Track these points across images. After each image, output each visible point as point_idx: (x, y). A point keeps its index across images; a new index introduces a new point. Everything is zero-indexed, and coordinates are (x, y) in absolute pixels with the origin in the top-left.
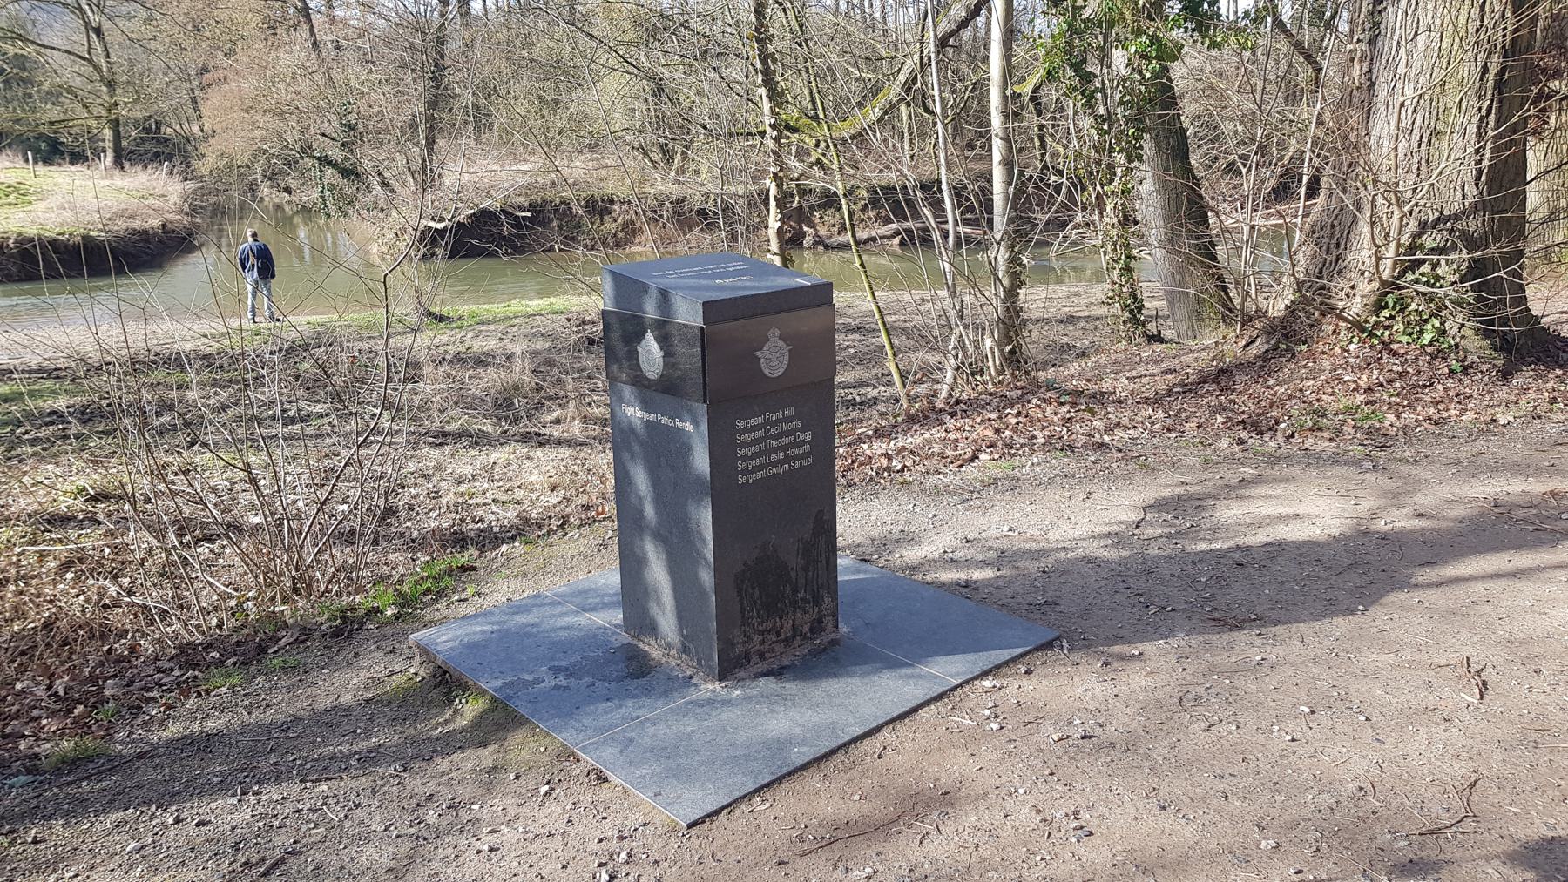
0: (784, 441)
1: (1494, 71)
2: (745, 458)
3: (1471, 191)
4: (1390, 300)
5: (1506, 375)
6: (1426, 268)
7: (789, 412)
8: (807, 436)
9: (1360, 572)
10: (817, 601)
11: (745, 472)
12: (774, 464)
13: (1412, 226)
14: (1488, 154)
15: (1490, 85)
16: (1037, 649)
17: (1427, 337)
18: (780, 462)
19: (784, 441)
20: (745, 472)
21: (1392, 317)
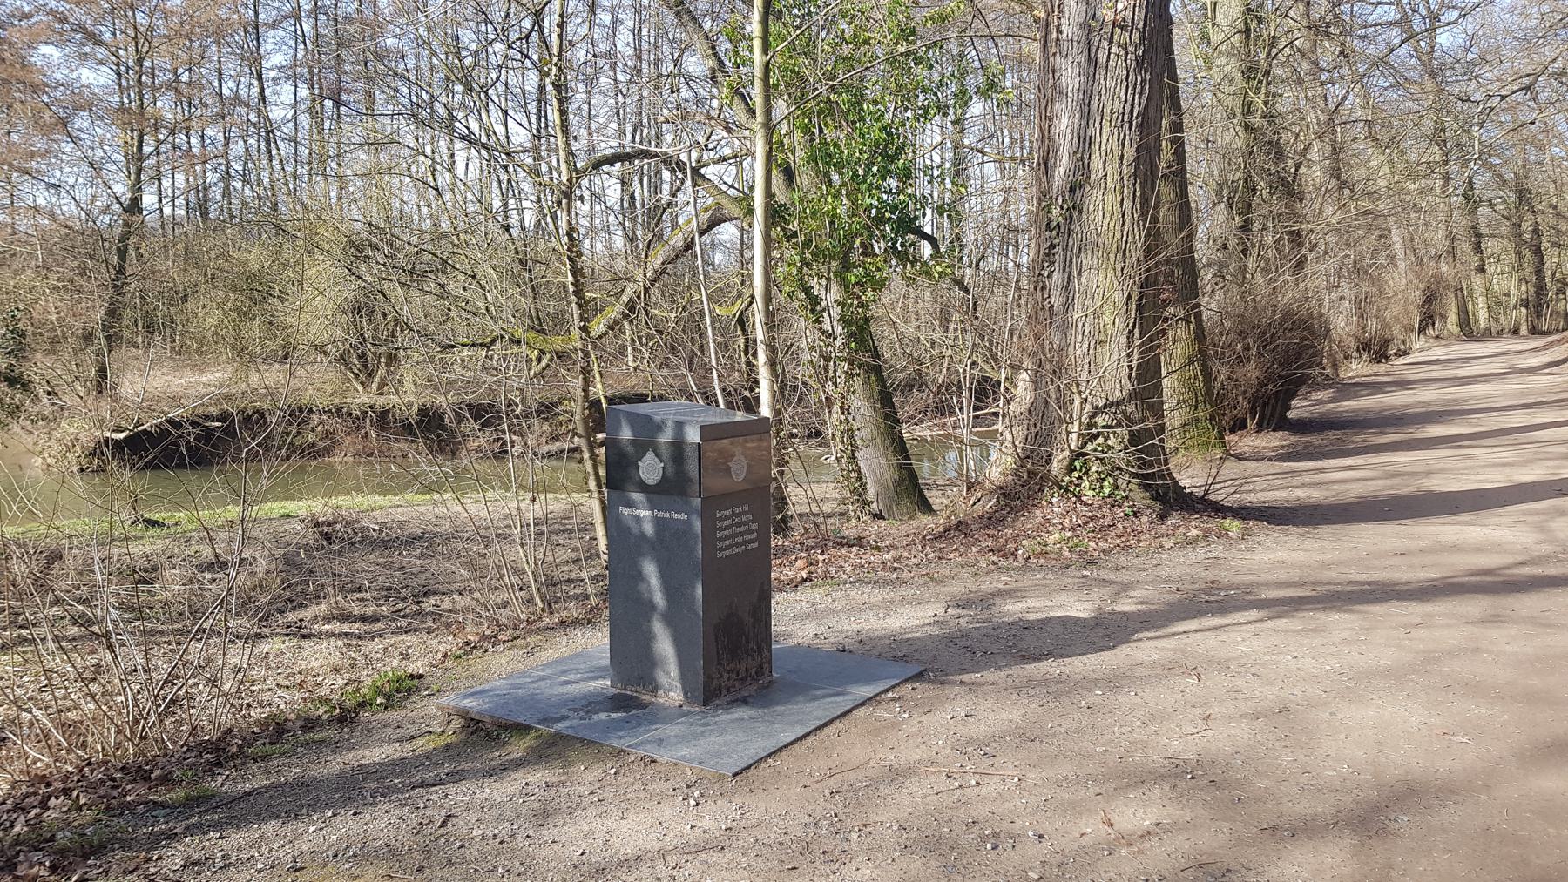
0: (742, 529)
1: (1135, 297)
2: (721, 539)
3: (1126, 383)
4: (1077, 464)
5: (1163, 517)
6: (1100, 440)
7: (746, 508)
8: (755, 526)
9: (1108, 631)
10: (760, 652)
11: (722, 549)
12: (737, 545)
13: (1088, 408)
14: (1136, 356)
15: (1134, 307)
16: (907, 680)
17: (1107, 491)
18: (741, 544)
19: (742, 529)
20: (722, 549)
21: (1080, 478)
